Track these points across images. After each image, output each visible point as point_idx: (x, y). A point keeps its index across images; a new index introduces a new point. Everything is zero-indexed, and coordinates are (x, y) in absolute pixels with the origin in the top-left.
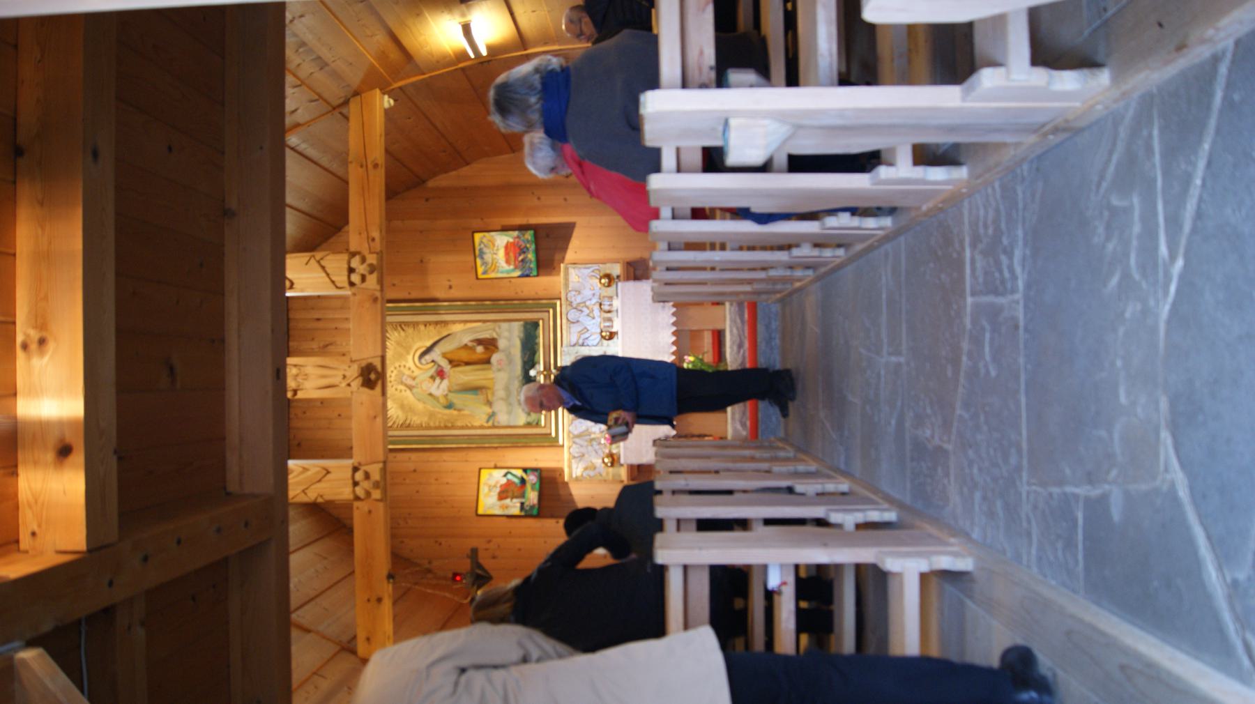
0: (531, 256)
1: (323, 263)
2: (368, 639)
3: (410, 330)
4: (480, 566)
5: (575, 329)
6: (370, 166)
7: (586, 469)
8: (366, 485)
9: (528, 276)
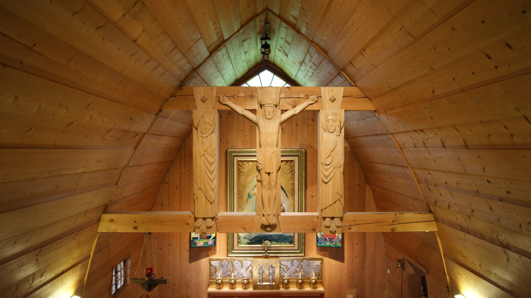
0: (328, 244)
1: (338, 202)
2: (112, 220)
3: (290, 176)
4: (156, 285)
5: (289, 264)
6: (393, 226)
7: (215, 267)
8: (203, 227)
9: (317, 241)
